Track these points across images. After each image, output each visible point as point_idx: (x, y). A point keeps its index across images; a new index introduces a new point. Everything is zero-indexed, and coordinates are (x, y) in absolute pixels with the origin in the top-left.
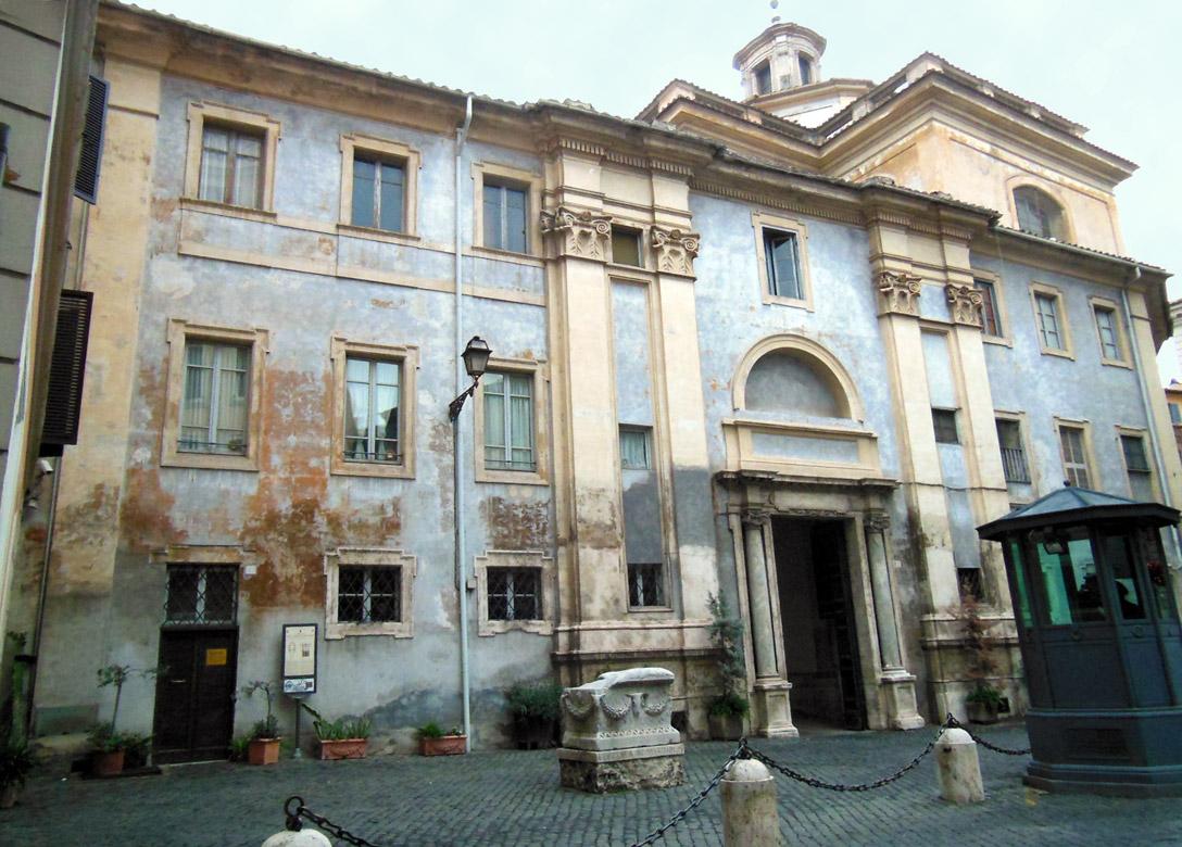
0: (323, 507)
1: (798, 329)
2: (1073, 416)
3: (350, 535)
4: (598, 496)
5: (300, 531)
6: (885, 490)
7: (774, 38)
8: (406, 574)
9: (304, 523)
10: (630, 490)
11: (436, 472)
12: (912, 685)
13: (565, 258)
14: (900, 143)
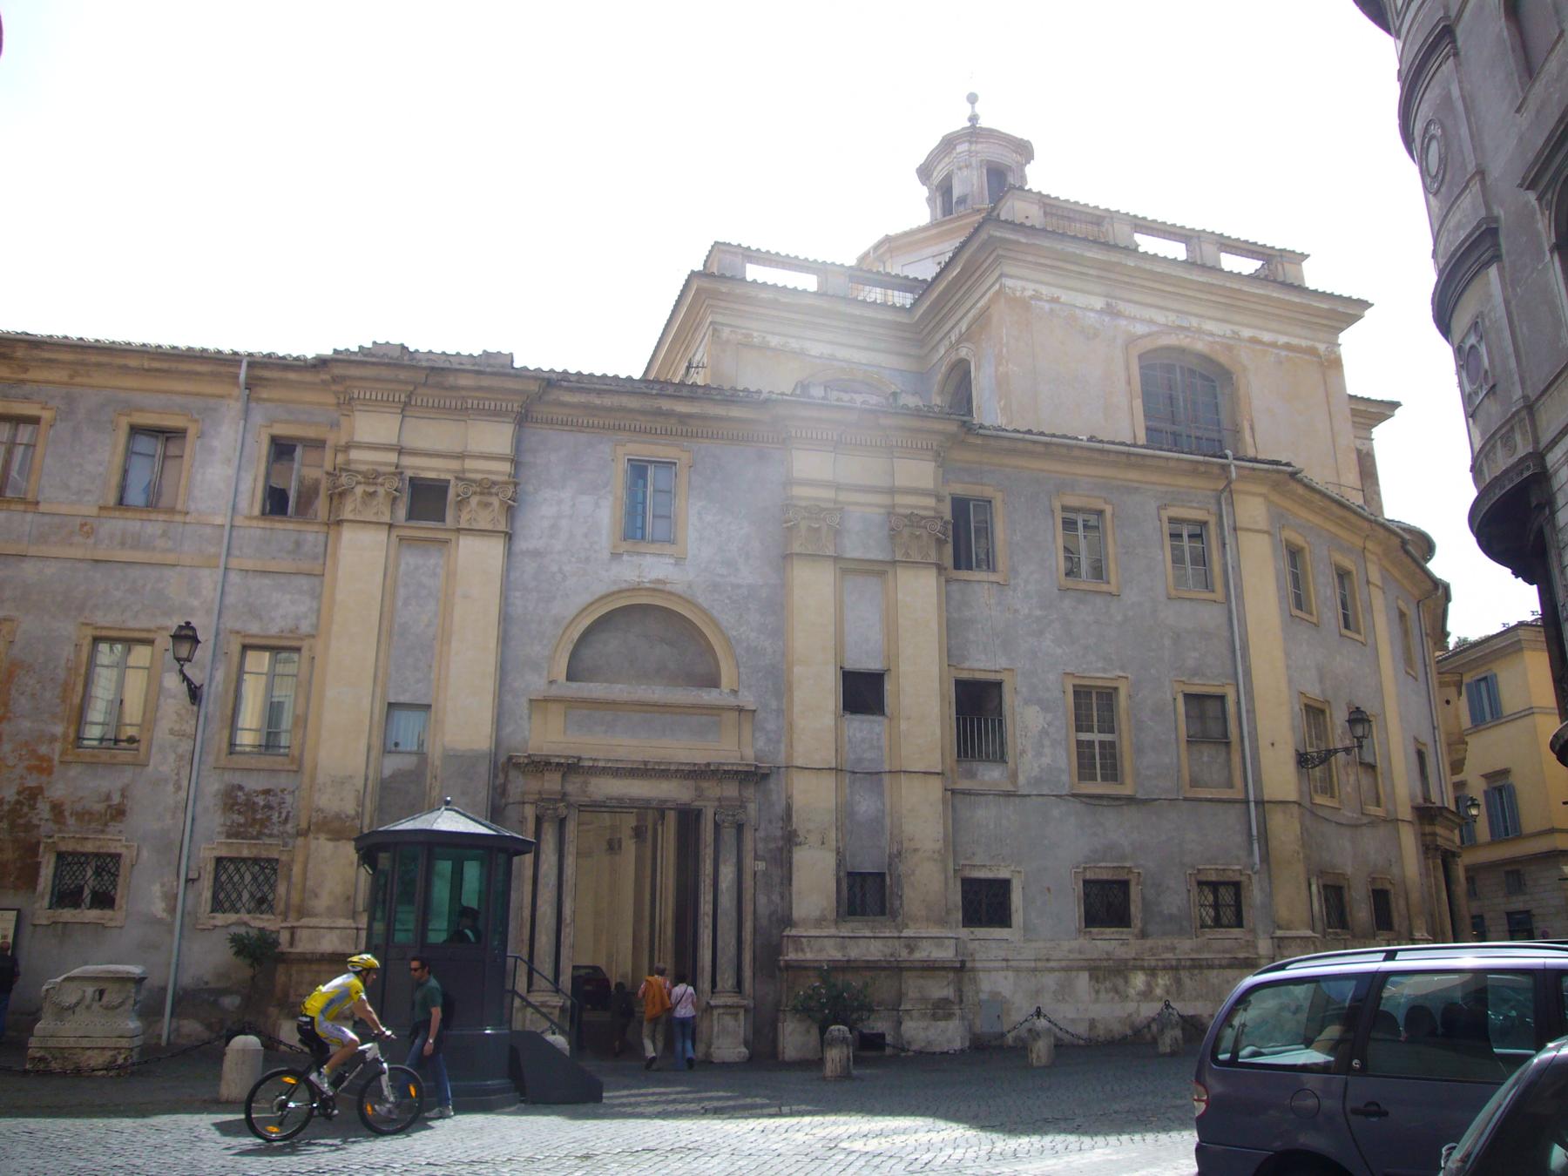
0: (47, 794)
1: (658, 581)
2: (1097, 672)
3: (71, 821)
4: (343, 783)
5: (20, 817)
6: (755, 776)
7: (954, 148)
8: (125, 862)
9: (25, 809)
10: (391, 777)
11: (172, 757)
12: (742, 1012)
13: (339, 523)
14: (979, 305)
